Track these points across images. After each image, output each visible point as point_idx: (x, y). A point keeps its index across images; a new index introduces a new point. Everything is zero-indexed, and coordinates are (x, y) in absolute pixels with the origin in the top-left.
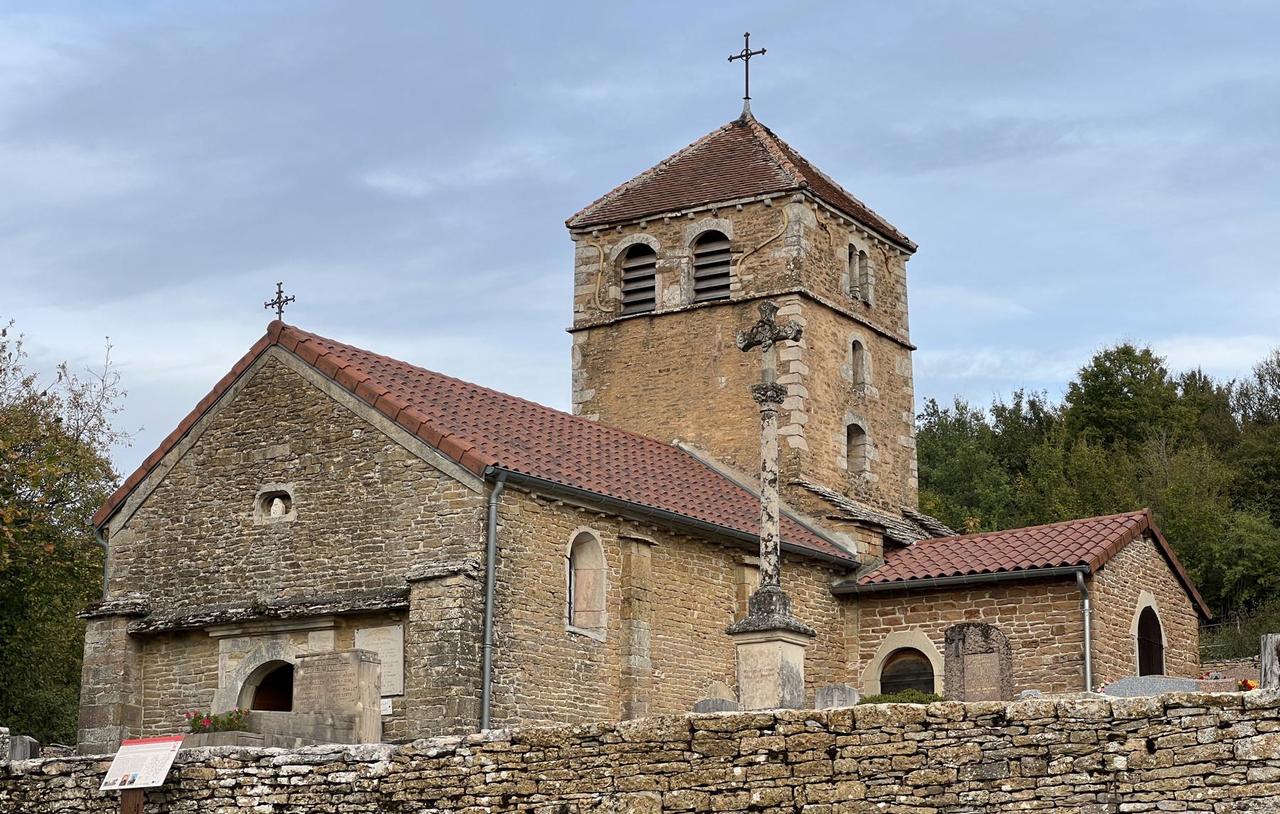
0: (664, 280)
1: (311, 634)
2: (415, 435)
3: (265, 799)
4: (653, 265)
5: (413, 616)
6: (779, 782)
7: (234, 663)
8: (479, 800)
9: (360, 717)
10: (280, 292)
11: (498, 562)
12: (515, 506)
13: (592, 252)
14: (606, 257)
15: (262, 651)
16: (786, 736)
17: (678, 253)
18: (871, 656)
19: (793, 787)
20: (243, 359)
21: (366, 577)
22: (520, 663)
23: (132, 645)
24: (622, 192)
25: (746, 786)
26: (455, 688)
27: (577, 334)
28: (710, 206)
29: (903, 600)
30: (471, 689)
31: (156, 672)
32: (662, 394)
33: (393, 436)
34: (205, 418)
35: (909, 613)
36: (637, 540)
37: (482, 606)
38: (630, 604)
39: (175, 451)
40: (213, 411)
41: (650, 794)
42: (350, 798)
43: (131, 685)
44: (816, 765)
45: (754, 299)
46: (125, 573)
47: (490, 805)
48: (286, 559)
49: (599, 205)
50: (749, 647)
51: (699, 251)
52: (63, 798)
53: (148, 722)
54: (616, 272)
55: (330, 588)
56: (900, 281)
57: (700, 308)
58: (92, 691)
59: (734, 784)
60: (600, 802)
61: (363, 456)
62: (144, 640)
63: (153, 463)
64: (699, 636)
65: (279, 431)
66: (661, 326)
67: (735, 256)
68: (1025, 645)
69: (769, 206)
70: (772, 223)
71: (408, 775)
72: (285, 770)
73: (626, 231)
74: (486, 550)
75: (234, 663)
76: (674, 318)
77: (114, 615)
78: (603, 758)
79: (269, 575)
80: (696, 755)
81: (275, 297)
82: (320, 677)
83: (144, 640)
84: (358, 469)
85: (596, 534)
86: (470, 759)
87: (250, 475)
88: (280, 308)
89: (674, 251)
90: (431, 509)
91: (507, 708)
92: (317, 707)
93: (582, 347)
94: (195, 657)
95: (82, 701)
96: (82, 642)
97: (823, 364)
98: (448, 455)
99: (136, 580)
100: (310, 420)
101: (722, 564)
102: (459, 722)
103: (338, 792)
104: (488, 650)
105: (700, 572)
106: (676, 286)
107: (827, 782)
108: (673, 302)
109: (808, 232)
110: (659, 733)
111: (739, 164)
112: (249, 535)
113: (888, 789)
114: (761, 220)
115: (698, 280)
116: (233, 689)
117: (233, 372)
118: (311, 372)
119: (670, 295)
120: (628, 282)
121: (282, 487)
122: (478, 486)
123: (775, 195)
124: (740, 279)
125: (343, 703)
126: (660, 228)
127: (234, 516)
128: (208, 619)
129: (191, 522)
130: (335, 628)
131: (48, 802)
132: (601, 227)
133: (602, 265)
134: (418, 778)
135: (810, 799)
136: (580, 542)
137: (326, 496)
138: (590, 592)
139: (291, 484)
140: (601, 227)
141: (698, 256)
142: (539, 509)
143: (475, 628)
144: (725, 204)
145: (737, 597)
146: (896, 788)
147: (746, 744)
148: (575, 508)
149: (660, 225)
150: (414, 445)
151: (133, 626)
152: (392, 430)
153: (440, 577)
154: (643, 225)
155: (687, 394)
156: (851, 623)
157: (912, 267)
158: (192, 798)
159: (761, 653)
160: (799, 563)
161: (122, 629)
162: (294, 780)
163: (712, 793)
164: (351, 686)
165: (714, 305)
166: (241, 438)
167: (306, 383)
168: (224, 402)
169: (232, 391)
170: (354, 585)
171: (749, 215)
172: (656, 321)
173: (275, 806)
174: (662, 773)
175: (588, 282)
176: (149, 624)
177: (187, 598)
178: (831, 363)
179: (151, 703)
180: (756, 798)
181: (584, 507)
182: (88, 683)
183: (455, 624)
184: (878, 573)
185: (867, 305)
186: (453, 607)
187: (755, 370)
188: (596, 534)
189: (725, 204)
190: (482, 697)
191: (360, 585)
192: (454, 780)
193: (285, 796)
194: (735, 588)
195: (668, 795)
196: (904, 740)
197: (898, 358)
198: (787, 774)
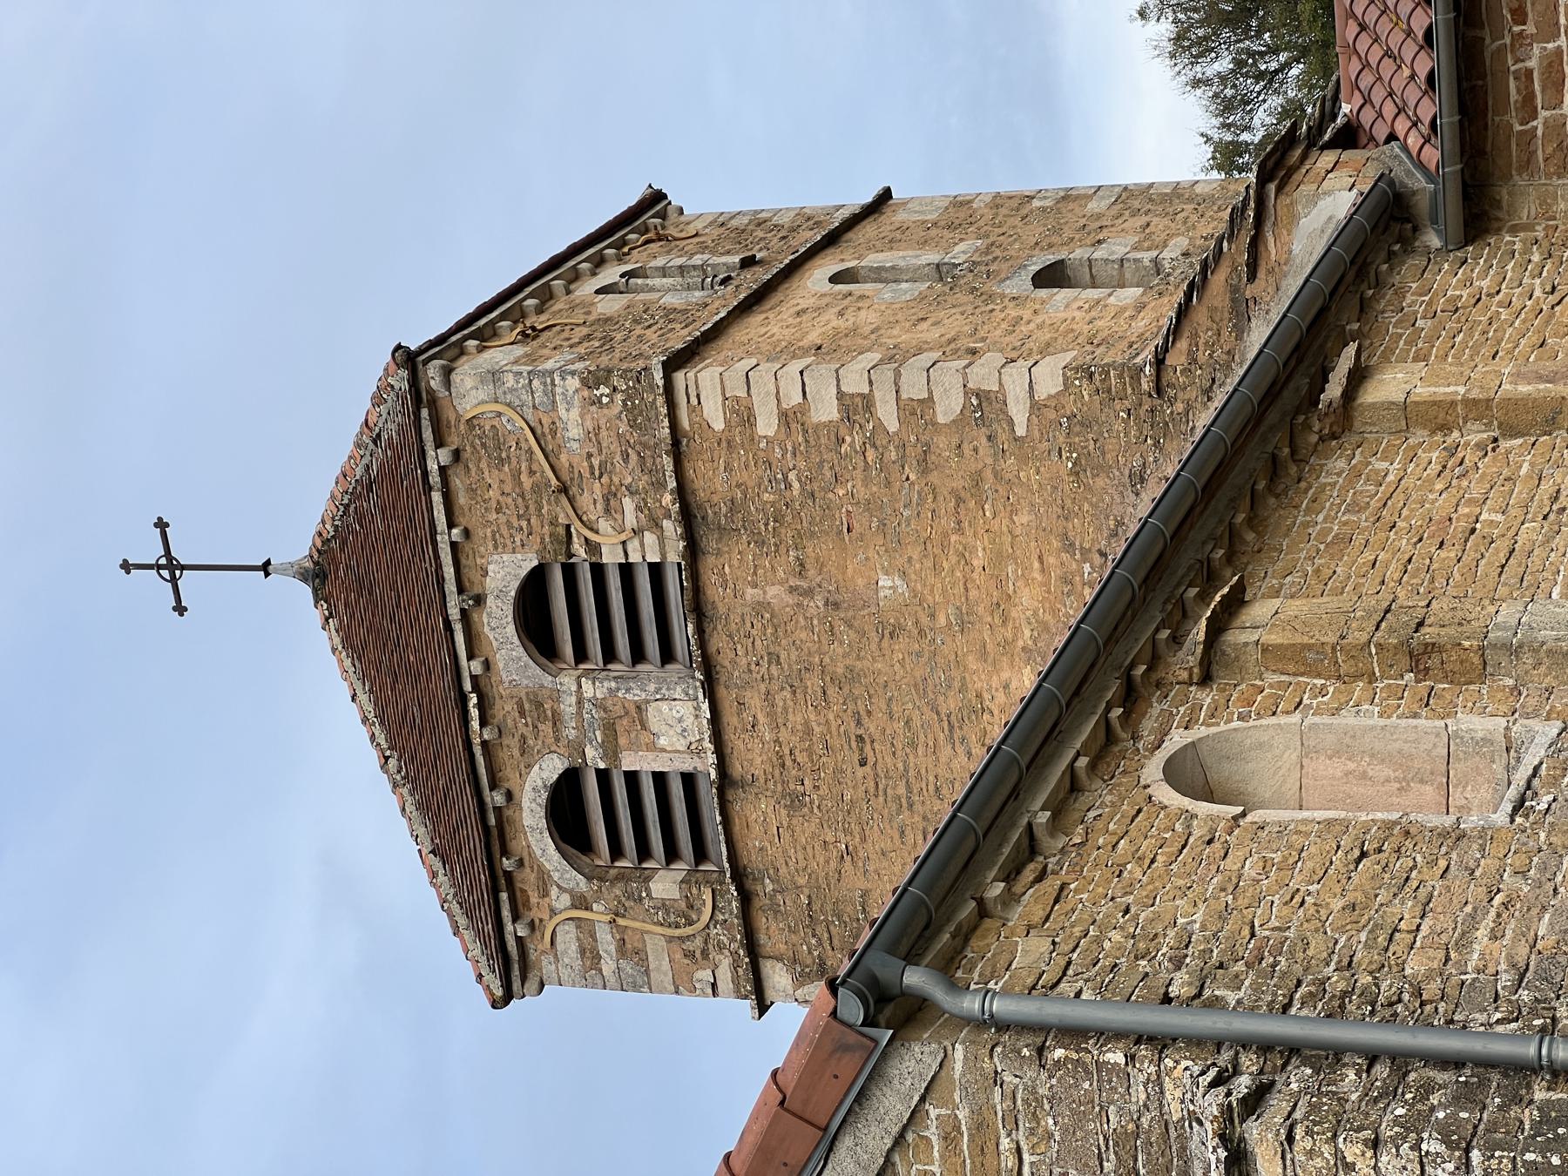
0: (634, 746)
4: (604, 777)
11: (1216, 1004)
12: (1021, 954)
13: (568, 940)
14: (581, 902)
17: (568, 706)
24: (437, 864)
27: (770, 995)
28: (454, 613)
29: (1491, 46)
32: (921, 759)
35: (1530, 28)
36: (1217, 628)
37: (1381, 1071)
38: (1431, 648)
45: (682, 492)
49: (462, 921)
51: (568, 650)
54: (618, 878)
56: (721, 222)
57: (702, 644)
66: (750, 757)
67: (579, 549)
69: (457, 455)
70: (496, 445)
73: (517, 845)
74: (1160, 1042)
76: (730, 719)
97: (868, 329)
101: (1341, 464)
105: (1356, 508)
106: (651, 710)
108: (689, 721)
109: (531, 359)
114: (492, 477)
115: (638, 655)
119: (670, 729)
120: (644, 852)
122: (914, 1063)
123: (428, 434)
124: (630, 536)
126: (509, 753)
132: (506, 913)
133: (599, 913)
138: (1381, 771)
140: (506, 913)
141: (581, 655)
142: (1051, 885)
143: (1467, 1096)
144: (449, 572)
145: (1445, 428)
148: (1073, 785)
149: (503, 755)
154: (498, 798)
155: (921, 687)
157: (698, 198)
160: (1364, 307)
165: (698, 609)
171: (479, 509)
172: (736, 770)
175: (640, 956)
187: (862, 493)
188: (1178, 739)
189: (449, 572)
194: (1419, 435)
197: (901, 217)
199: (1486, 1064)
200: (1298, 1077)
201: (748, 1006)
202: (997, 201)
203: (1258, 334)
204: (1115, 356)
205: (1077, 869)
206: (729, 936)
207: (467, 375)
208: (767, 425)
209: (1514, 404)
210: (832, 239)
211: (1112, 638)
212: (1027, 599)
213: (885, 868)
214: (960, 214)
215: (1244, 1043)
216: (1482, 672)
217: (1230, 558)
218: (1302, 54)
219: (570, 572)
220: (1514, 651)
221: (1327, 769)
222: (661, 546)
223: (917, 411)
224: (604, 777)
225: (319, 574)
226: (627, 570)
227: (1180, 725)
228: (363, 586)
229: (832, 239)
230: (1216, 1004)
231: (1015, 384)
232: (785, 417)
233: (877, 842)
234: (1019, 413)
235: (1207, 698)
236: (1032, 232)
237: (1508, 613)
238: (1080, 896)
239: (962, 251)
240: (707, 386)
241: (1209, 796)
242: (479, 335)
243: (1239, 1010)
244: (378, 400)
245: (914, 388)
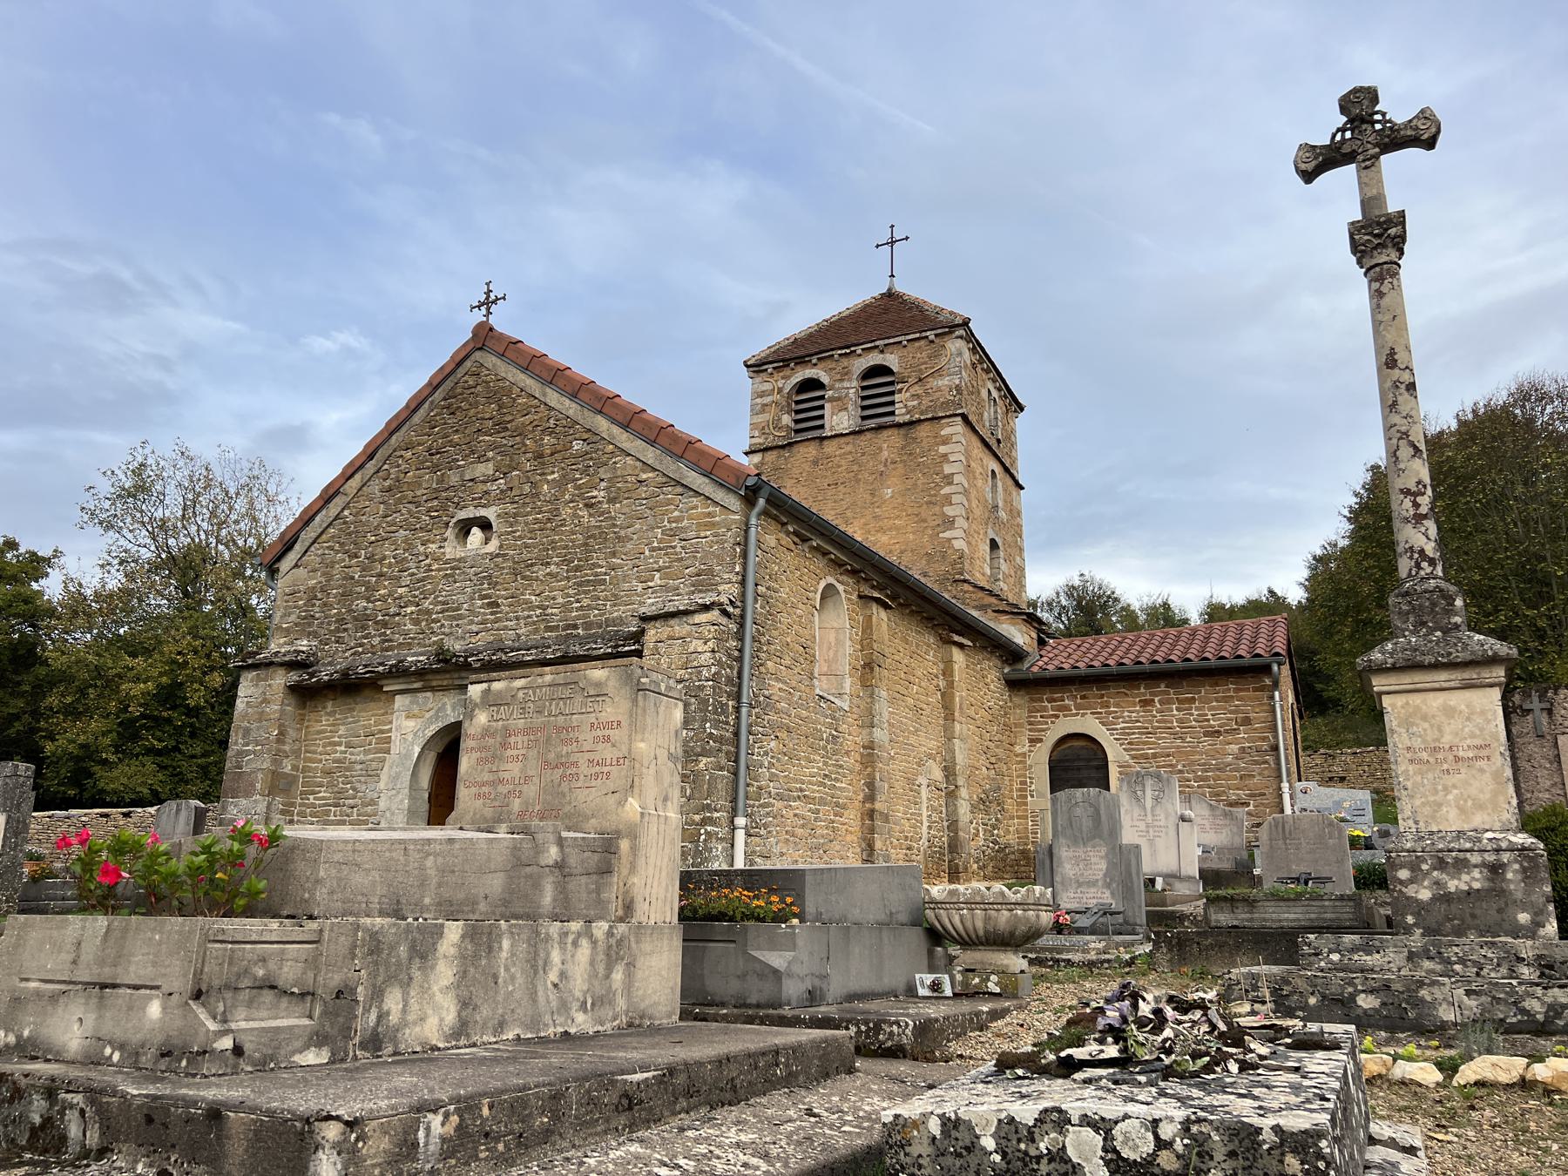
2: (652, 443)
4: (822, 397)
9: (633, 835)
11: (756, 601)
12: (768, 537)
13: (767, 386)
14: (780, 390)
17: (846, 384)
18: (1041, 741)
21: (585, 617)
22: (775, 730)
23: (291, 700)
26: (704, 760)
30: (723, 761)
31: (319, 732)
32: (830, 505)
33: (625, 445)
36: (877, 600)
37: (736, 653)
38: (872, 669)
39: (358, 477)
40: (404, 429)
43: (287, 748)
45: (920, 421)
46: (293, 618)
50: (1416, 699)
53: (306, 793)
55: (536, 631)
56: (1013, 431)
58: (240, 753)
61: (585, 471)
62: (307, 694)
63: (331, 492)
64: (917, 710)
65: (481, 447)
66: (830, 447)
70: (935, 356)
74: (743, 583)
75: (411, 724)
76: (843, 440)
77: (271, 664)
79: (460, 617)
82: (527, 731)
83: (307, 694)
84: (578, 488)
87: (444, 499)
88: (488, 309)
90: (672, 534)
91: (760, 788)
92: (516, 804)
94: (365, 716)
95: (228, 765)
96: (235, 696)
98: (695, 466)
99: (304, 626)
102: (708, 808)
104: (744, 710)
112: (439, 570)
116: (408, 756)
117: (430, 383)
118: (522, 376)
119: (839, 420)
120: (797, 412)
121: (482, 512)
122: (733, 503)
124: (904, 404)
125: (587, 797)
127: (422, 549)
128: (381, 669)
129: (370, 558)
133: (777, 397)
137: (537, 521)
138: (831, 653)
139: (494, 508)
141: (863, 388)
142: (793, 547)
143: (729, 681)
148: (825, 554)
150: (650, 455)
151: (294, 677)
152: (623, 439)
153: (686, 613)
157: (1021, 423)
159: (1450, 712)
160: (985, 648)
161: (280, 680)
164: (608, 753)
167: (516, 390)
168: (416, 419)
169: (426, 405)
170: (568, 627)
172: (826, 442)
175: (763, 411)
176: (312, 675)
177: (361, 645)
179: (310, 769)
181: (836, 553)
182: (236, 743)
183: (705, 673)
184: (1039, 663)
186: (703, 652)
188: (841, 588)
190: (736, 774)
191: (575, 627)
194: (941, 666)
199: (740, 686)
200: (734, 627)
201: (747, 449)
202: (1020, 526)
203: (975, 613)
204: (967, 566)
205: (798, 555)
206: (770, 442)
207: (960, 344)
208: (942, 449)
209: (952, 696)
210: (1007, 470)
211: (873, 566)
212: (885, 539)
213: (797, 492)
214: (1015, 513)
215: (744, 610)
216: (864, 686)
217: (900, 605)
218: (1067, 628)
219: (892, 383)
220: (871, 696)
221: (832, 637)
223: (948, 500)
224: (822, 397)
225: (890, 295)
226: (892, 403)
227: (845, 589)
228: (886, 311)
229: (1007, 470)
230: (756, 601)
231: (958, 533)
232: (945, 455)
233: (803, 490)
234: (947, 534)
235: (854, 597)
236: (1009, 538)
237: (884, 694)
238: (789, 556)
239: (1002, 514)
240: (956, 428)
243: (754, 608)
244: (951, 313)
245: (956, 499)
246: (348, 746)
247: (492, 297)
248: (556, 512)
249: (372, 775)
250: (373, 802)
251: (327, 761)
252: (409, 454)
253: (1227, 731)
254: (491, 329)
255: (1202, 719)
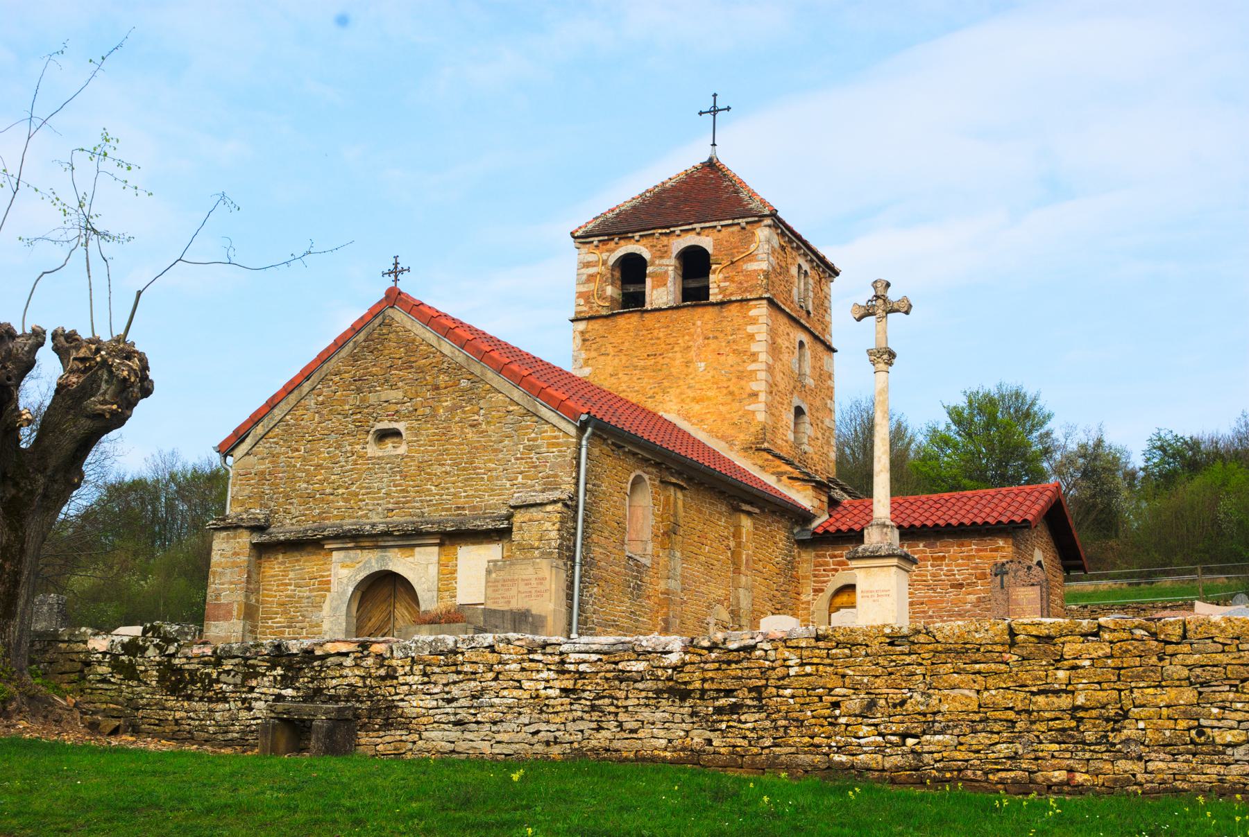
1: (417, 549)
3: (551, 683)
5: (516, 536)
6: (1105, 686)
7: (344, 572)
8: (781, 692)
10: (396, 264)
13: (592, 258)
14: (605, 263)
15: (371, 562)
16: (1111, 642)
17: (665, 261)
18: (822, 590)
19: (1120, 691)
20: (362, 318)
25: (1069, 688)
27: (576, 323)
28: (695, 226)
31: (273, 576)
34: (325, 366)
36: (674, 485)
40: (333, 361)
41: (966, 692)
42: (640, 685)
44: (1144, 671)
45: (730, 302)
47: (793, 697)
48: (395, 486)
52: (341, 676)
59: (1056, 686)
60: (911, 697)
64: (709, 566)
68: (952, 586)
69: (743, 228)
71: (707, 666)
72: (573, 657)
78: (914, 657)
80: (1016, 658)
81: (392, 268)
85: (646, 477)
86: (772, 653)
89: (662, 257)
93: (582, 333)
94: (308, 564)
100: (421, 370)
103: (628, 679)
105: (710, 514)
107: (1155, 687)
110: (977, 636)
111: (709, 194)
113: (1224, 696)
116: (344, 592)
124: (717, 283)
127: (349, 448)
130: (441, 545)
131: (324, 679)
134: (718, 669)
135: (1137, 702)
136: (637, 482)
144: (707, 225)
146: (1231, 695)
147: (1069, 650)
148: (635, 454)
150: (517, 394)
154: (637, 238)
156: (807, 560)
157: (836, 286)
158: (475, 680)
160: (774, 512)
161: (245, 539)
162: (582, 667)
163: (1033, 693)
166: (359, 384)
168: (344, 352)
169: (351, 344)
170: (458, 508)
172: (646, 315)
173: (562, 690)
174: (979, 673)
178: (785, 357)
179: (267, 602)
180: (1080, 700)
185: (808, 313)
188: (646, 477)
189: (707, 225)
191: (463, 508)
192: (756, 672)
193: (572, 682)
194: (732, 529)
195: (986, 694)
196: (1239, 650)
197: (825, 357)
198: (1114, 678)
201: (572, 316)
202: (830, 389)
208: (750, 329)
209: (740, 554)
210: (816, 338)
222: (715, 295)
229: (816, 338)
235: (657, 483)
236: (818, 403)
238: (608, 460)
241: (633, 484)
242: (782, 231)
244: (763, 201)
246: (297, 586)
247: (399, 267)
248: (448, 429)
249: (318, 606)
250: (318, 625)
251: (280, 596)
252: (337, 379)
253: (968, 584)
254: (400, 293)
255: (950, 573)
